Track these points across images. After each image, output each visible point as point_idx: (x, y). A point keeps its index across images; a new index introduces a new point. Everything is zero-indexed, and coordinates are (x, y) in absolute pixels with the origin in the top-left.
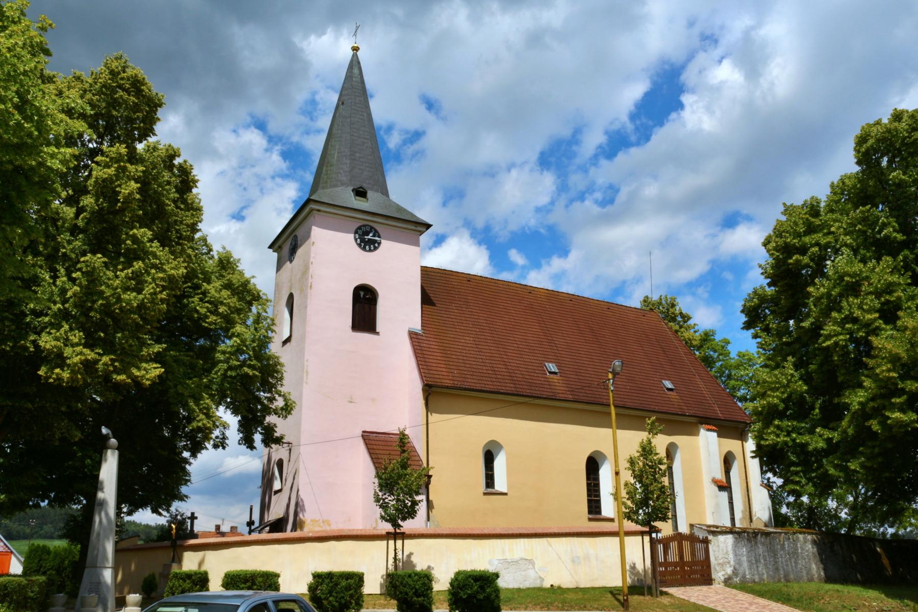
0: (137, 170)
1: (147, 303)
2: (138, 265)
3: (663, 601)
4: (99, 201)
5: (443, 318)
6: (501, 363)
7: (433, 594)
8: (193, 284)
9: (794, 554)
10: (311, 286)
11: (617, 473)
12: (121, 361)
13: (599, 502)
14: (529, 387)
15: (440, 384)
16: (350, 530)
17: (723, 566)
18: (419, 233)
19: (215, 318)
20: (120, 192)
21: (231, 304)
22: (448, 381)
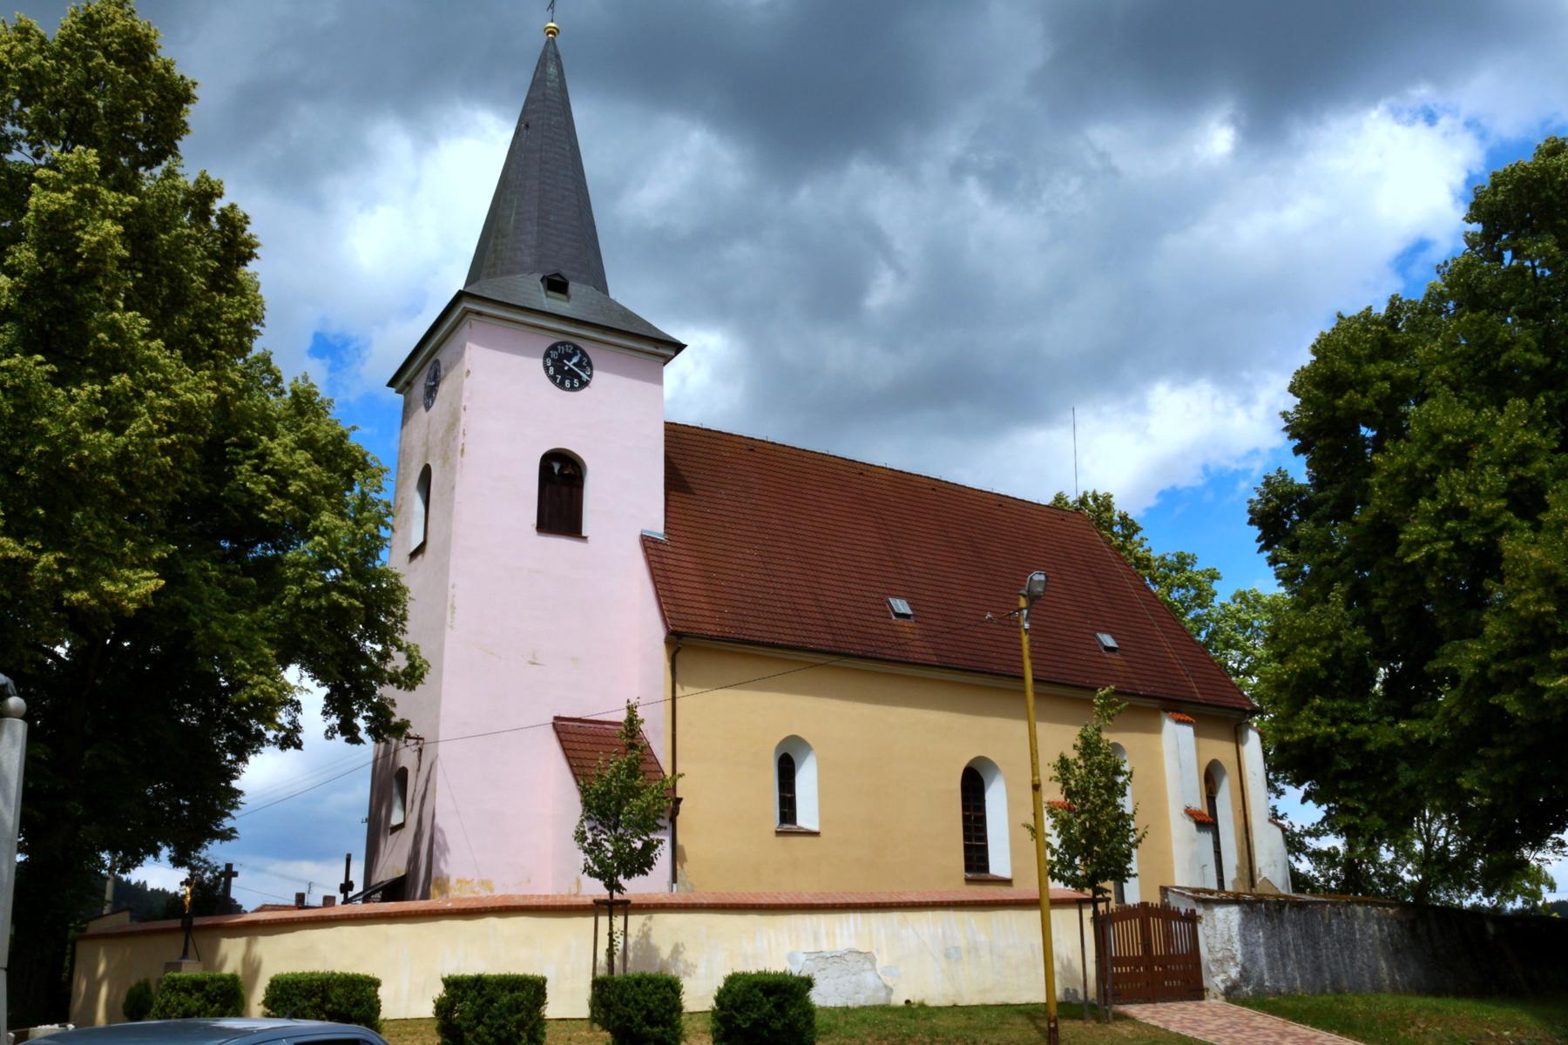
0: (121, 201)
1: (133, 452)
2: (120, 381)
3: (1120, 1031)
4: (44, 255)
5: (705, 515)
6: (810, 596)
7: (683, 1018)
8: (241, 438)
9: (1349, 942)
10: (462, 450)
11: (1036, 787)
12: (82, 564)
13: (984, 849)
14: (860, 641)
15: (697, 631)
16: (525, 897)
17: (1222, 964)
18: (662, 360)
19: (282, 503)
20: (82, 240)
21: (313, 477)
22: (713, 627)
